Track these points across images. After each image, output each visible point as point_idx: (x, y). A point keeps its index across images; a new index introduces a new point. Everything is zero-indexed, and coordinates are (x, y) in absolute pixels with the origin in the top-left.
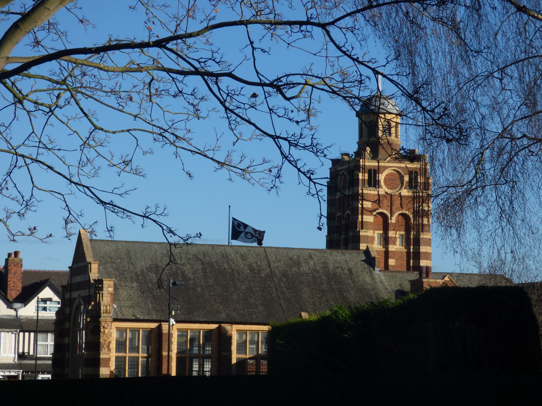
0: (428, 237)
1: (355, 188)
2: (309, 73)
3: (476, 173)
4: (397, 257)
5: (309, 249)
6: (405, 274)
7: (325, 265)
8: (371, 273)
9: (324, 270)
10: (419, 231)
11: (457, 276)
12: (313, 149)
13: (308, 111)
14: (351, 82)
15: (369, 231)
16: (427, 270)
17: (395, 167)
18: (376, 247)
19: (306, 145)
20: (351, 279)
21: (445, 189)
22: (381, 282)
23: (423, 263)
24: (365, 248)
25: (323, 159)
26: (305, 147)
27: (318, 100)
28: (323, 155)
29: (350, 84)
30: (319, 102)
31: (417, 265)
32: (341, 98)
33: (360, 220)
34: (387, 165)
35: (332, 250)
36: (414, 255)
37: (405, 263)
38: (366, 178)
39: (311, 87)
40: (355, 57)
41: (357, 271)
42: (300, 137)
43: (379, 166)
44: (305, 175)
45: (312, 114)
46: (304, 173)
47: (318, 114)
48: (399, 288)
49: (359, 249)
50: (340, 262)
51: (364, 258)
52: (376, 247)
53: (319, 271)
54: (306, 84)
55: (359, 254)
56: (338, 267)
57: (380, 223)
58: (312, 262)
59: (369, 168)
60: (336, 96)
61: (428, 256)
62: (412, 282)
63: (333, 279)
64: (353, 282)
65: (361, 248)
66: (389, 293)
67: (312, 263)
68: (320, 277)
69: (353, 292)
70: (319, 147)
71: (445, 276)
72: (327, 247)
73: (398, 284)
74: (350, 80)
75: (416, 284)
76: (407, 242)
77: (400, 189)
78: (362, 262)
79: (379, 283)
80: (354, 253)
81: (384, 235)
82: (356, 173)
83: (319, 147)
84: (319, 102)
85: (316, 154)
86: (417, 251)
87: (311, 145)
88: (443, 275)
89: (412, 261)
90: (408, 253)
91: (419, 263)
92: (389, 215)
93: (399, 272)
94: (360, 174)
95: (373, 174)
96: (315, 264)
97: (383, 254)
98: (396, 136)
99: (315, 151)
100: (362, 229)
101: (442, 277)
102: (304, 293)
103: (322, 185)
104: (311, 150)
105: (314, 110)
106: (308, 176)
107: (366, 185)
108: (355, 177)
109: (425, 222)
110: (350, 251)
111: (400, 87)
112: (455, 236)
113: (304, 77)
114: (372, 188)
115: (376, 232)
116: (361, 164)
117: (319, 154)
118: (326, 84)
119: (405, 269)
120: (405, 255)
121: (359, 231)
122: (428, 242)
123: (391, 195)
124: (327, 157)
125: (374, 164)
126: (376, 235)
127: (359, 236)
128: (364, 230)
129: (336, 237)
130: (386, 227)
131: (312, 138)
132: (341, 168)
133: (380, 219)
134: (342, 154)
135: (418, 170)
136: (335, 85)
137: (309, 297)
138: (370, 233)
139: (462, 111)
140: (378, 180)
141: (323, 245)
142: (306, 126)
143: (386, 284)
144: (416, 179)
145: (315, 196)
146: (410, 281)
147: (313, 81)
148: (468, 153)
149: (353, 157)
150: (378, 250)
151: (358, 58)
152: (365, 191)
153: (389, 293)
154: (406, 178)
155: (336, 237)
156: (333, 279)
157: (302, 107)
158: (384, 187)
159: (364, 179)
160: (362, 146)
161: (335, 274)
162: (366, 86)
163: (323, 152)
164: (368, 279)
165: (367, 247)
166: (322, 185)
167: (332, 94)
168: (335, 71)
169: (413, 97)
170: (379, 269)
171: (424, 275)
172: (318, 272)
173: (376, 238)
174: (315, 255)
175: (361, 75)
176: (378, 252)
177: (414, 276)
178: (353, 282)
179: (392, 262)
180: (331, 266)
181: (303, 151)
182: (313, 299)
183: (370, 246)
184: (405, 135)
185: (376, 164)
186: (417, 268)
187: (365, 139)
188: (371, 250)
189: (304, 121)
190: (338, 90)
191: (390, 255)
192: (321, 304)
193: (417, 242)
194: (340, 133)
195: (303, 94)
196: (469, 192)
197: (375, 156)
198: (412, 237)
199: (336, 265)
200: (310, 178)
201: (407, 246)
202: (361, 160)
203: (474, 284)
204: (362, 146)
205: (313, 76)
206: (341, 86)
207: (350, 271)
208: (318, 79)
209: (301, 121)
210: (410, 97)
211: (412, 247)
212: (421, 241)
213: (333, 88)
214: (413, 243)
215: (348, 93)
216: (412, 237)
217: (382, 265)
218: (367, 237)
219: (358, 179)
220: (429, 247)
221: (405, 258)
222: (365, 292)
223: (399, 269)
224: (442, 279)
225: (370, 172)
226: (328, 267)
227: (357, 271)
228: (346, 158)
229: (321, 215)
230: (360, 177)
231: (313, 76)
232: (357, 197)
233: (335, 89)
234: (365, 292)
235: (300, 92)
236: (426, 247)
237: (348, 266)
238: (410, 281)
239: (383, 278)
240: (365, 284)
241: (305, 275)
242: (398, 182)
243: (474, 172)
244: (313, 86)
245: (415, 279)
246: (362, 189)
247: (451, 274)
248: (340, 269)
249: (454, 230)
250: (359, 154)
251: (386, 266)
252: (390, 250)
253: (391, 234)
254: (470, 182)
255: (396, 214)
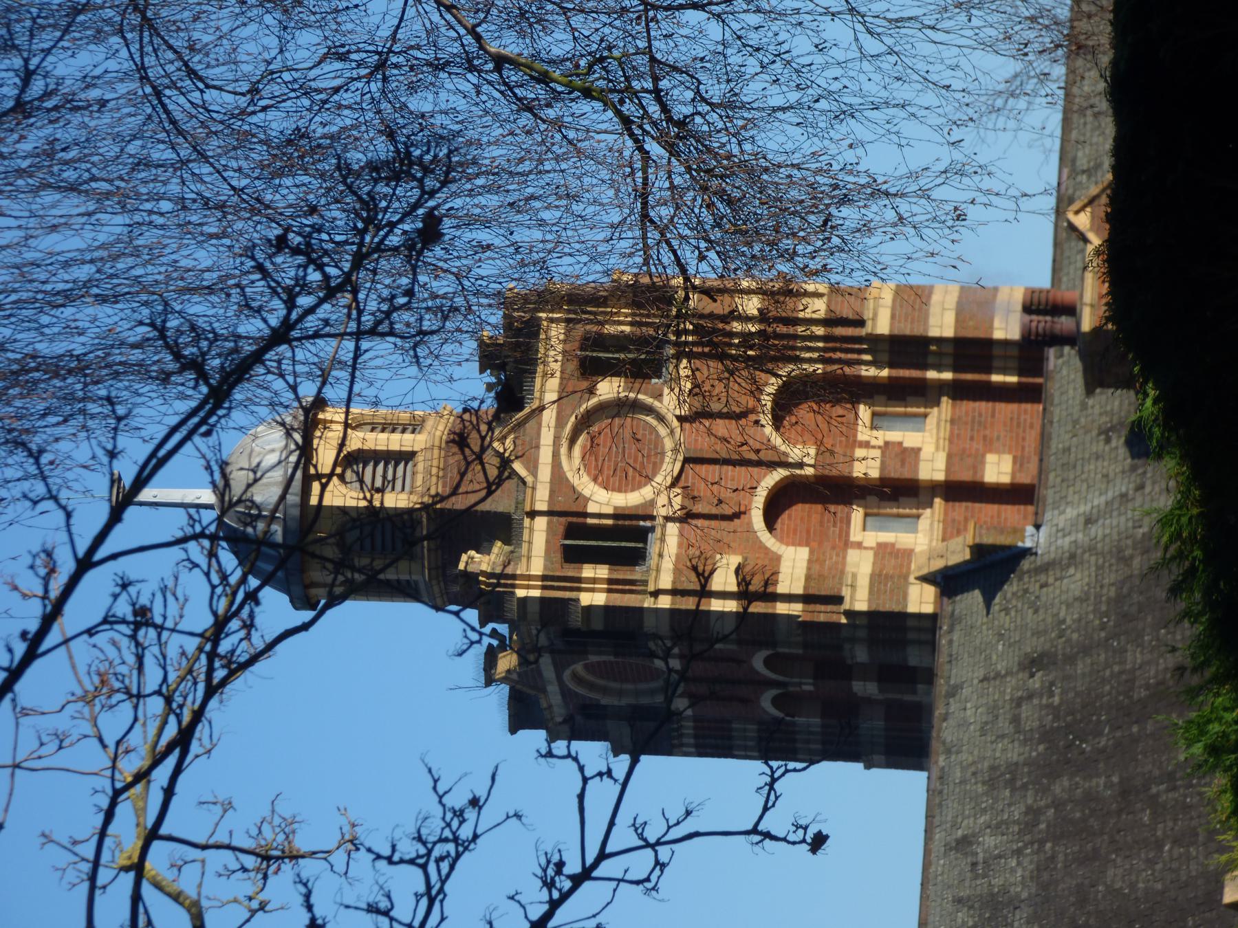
0: (887, 296)
1: (649, 624)
2: (88, 851)
3: (588, 93)
4: (977, 445)
5: (927, 852)
6: (1057, 412)
7: (1000, 778)
8: (1045, 568)
9: (1024, 787)
10: (859, 340)
11: (1074, 172)
12: (440, 860)
13: (267, 858)
14: (140, 659)
15: (849, 569)
16: (1038, 312)
17: (557, 438)
18: (926, 538)
19: (422, 888)
20: (1071, 659)
21: (653, 235)
22: (1089, 521)
23: (1007, 327)
24: (930, 591)
25: (491, 814)
26: (432, 896)
27: (218, 810)
28: (470, 814)
29: (149, 661)
30: (228, 806)
31: (1015, 352)
32: (213, 703)
33: (796, 609)
34: (545, 473)
35: (935, 745)
36: (970, 367)
37: (1005, 410)
38: (603, 571)
39: (156, 845)
40: (20, 648)
41: (1036, 634)
42: (386, 913)
43: (549, 513)
44: (565, 896)
45: (281, 837)
46: (554, 905)
47: (285, 809)
48: (1118, 442)
49: (933, 618)
50: (993, 710)
51: (976, 596)
52: (926, 538)
53: (1029, 810)
54: (138, 868)
55: (954, 620)
56: (1016, 720)
57: (815, 518)
58: (990, 841)
59: (558, 556)
60: (202, 731)
61: (976, 300)
62: (1096, 379)
63: (1069, 746)
64: (1086, 650)
65: (928, 609)
66: (1141, 487)
67: (990, 841)
68: (1058, 805)
69: (1135, 656)
70: (433, 829)
71: (1072, 227)
72: (920, 767)
73: (1100, 446)
74: (131, 660)
75: (1101, 370)
76: (906, 395)
77: (661, 419)
78: (995, 608)
79: (1096, 530)
80: (950, 641)
81: (872, 499)
82: (576, 621)
83: (433, 829)
84: (228, 806)
85: (464, 846)
86: (949, 349)
87: (424, 867)
88: (1067, 235)
89: (996, 378)
90: (959, 391)
91: (1006, 343)
92: (779, 474)
93: (1044, 438)
94: (586, 599)
95: (584, 539)
96: (997, 828)
97: (961, 509)
98: (415, 426)
99: (451, 847)
100: (839, 600)
101: (1077, 244)
102: (1133, 886)
103: (612, 824)
104: (445, 866)
105: (266, 828)
106: (567, 885)
107: (637, 573)
108: (598, 624)
109: (818, 308)
110: (942, 658)
111: (170, 445)
112: (878, 211)
113: (104, 876)
114: (653, 549)
115: (856, 534)
116: (536, 593)
117: (465, 832)
118: (142, 776)
119: (1031, 411)
120: (968, 406)
121: (849, 614)
122: (914, 298)
123: (687, 461)
124: (481, 793)
125: (538, 539)
126: (872, 538)
127: (871, 615)
128: (846, 592)
129: (873, 725)
130: (835, 490)
131: (390, 860)
132: (553, 689)
133: (798, 514)
134: (489, 681)
135: (580, 330)
136: (152, 730)
137: (1151, 862)
138: (860, 565)
139: (295, 150)
140: (615, 516)
141: (906, 788)
142: (340, 867)
143: (1099, 501)
144: (620, 343)
145: (663, 858)
146: (1089, 391)
147: (126, 832)
148: (495, 134)
149: (503, 629)
150: (938, 529)
151: (24, 635)
152: (666, 582)
153: (1141, 487)
154: (609, 388)
155: (873, 725)
156: (1069, 746)
157: (243, 886)
158: (647, 492)
159: (610, 581)
160: (456, 589)
161: (1046, 736)
162: (164, 590)
163: (459, 814)
164: (1076, 582)
165: (925, 579)
166: (612, 824)
167: (195, 748)
168: (87, 728)
169: (221, 381)
170: (1030, 529)
171: (1065, 323)
172: (1034, 813)
173: (887, 537)
174: (955, 825)
175: (109, 620)
176: (950, 530)
177: (1065, 367)
178: (1086, 650)
179: (998, 469)
180: (1013, 752)
181: (450, 905)
182: (1159, 846)
183: (920, 566)
184: (403, 410)
185: (541, 523)
186: (1030, 352)
187: (420, 574)
188: (938, 564)
189: (307, 896)
190: (172, 719)
191: (965, 476)
192: (1187, 808)
193: (907, 348)
194: (388, 697)
195: (187, 883)
196: (678, 133)
197: (504, 528)
198: (885, 373)
199: (1004, 725)
200: (578, 880)
201: (925, 394)
202: (521, 593)
203: (1101, 137)
204: (456, 589)
205: (103, 834)
206: (155, 705)
207: (1033, 664)
208: (119, 810)
209: (310, 908)
210: (219, 397)
211: (932, 374)
212: (907, 329)
213: (164, 741)
214: (914, 368)
215: (190, 671)
216: (885, 373)
217: (1011, 513)
218: (877, 579)
219: (607, 609)
220: (936, 298)
221: (983, 406)
222: (1136, 597)
223: (1032, 437)
224: (1086, 241)
225: (574, 556)
226: (1013, 768)
227: (1036, 634)
228: (507, 662)
229: (754, 831)
230: (599, 599)
231: (103, 834)
232: (690, 627)
233: (171, 731)
234: (1136, 597)
235: (177, 897)
236: (934, 309)
237: (1009, 673)
238: (1089, 391)
239: (1071, 513)
240: (1098, 596)
241: (1045, 876)
242: (628, 423)
243: (585, 106)
244: (153, 835)
245: (1077, 363)
246: (656, 594)
247: (1063, 203)
248: (1025, 711)
249: (845, 211)
250: (489, 598)
251: (1017, 494)
252: (940, 476)
253: (867, 467)
254: (626, 121)
255: (777, 440)
